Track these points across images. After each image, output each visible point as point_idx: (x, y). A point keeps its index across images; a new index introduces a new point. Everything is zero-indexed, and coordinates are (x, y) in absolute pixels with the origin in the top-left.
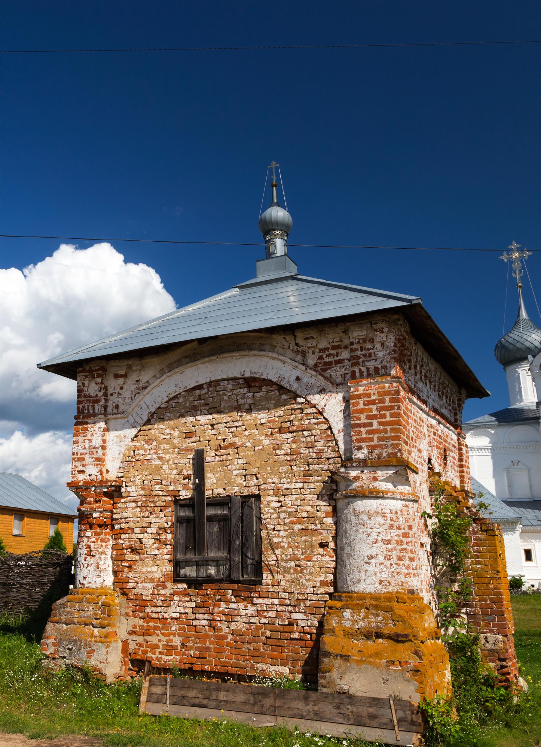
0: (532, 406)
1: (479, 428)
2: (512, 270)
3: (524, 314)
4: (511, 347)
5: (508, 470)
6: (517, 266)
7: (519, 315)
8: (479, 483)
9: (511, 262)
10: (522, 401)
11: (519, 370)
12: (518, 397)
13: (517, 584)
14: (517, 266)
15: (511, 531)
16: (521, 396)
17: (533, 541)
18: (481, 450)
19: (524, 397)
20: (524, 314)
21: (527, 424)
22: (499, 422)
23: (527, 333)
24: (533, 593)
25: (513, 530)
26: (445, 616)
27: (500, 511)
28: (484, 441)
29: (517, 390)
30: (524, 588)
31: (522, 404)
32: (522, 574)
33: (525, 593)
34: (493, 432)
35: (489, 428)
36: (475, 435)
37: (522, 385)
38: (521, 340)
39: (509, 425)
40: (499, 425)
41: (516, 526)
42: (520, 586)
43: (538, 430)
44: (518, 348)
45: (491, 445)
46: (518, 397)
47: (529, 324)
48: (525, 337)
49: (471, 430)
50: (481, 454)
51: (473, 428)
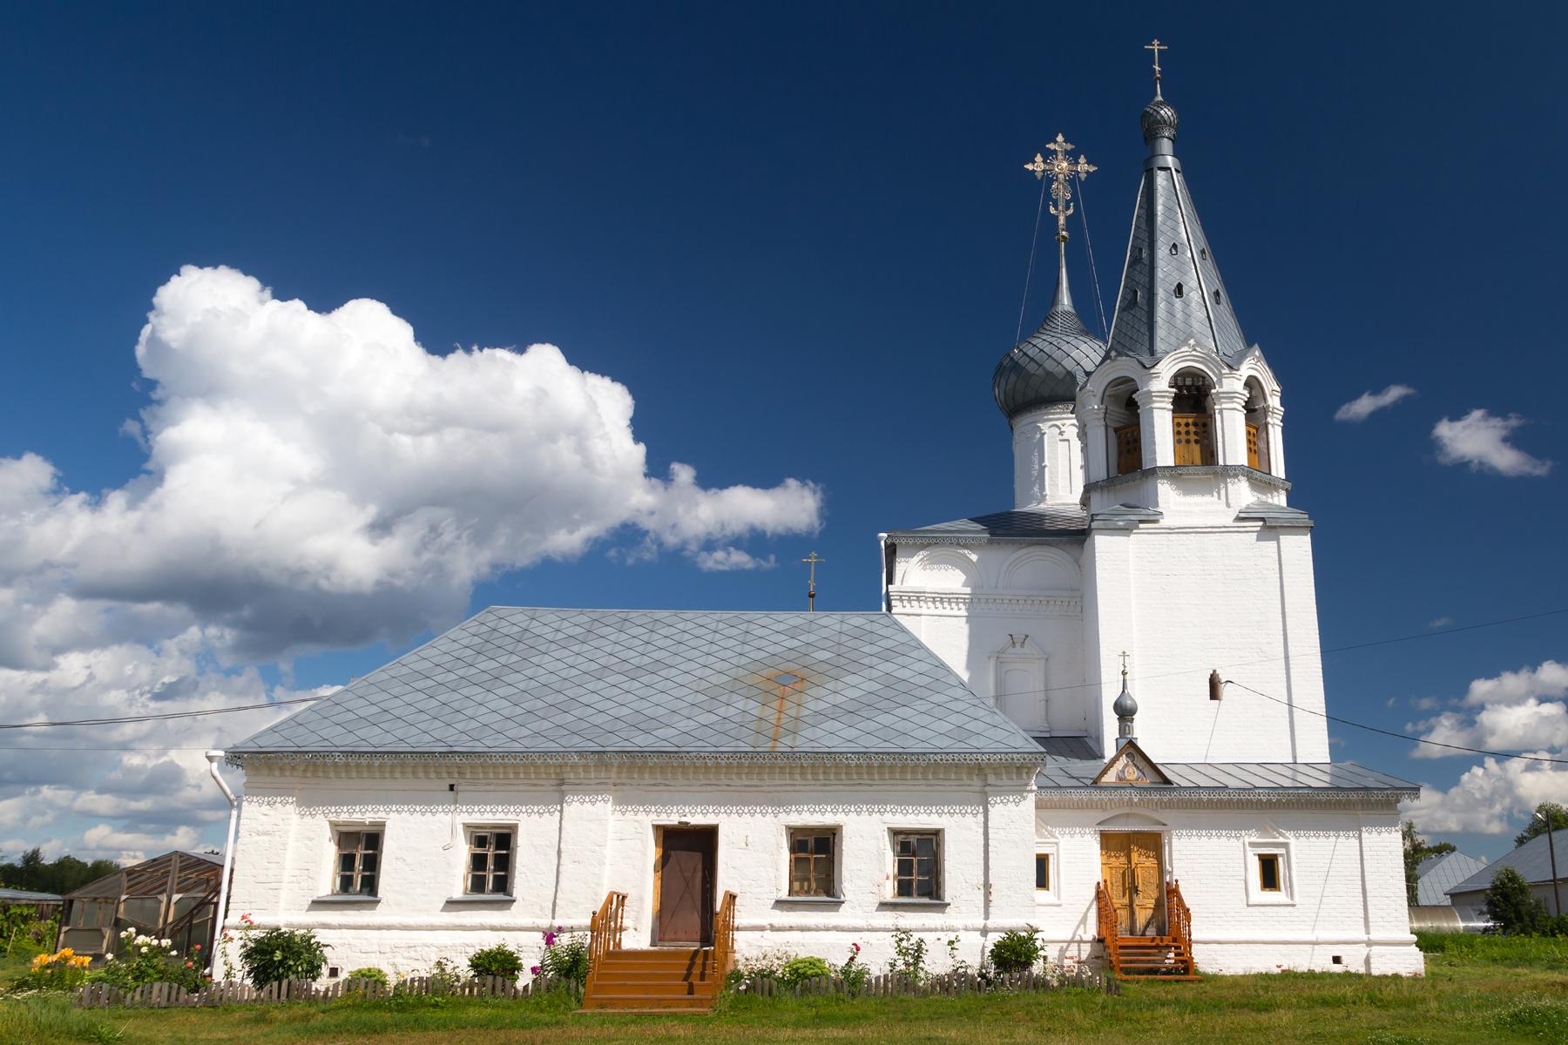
0: (1073, 508)
1: (943, 545)
2: (1050, 199)
3: (1065, 300)
4: (1032, 368)
5: (1000, 661)
6: (1061, 191)
7: (1054, 299)
8: (937, 658)
9: (1049, 179)
10: (1043, 498)
11: (1044, 427)
12: (1036, 489)
13: (1018, 955)
14: (1061, 191)
15: (1014, 792)
16: (1042, 488)
17: (1057, 831)
18: (942, 601)
19: (1047, 491)
20: (1065, 300)
21: (1056, 545)
22: (992, 534)
23: (1070, 339)
24: (1062, 984)
25: (1021, 791)
26: (1452, 1010)
27: (990, 732)
28: (951, 580)
29: (1035, 473)
30: (1037, 968)
31: (1042, 506)
32: (1035, 923)
33: (1040, 984)
34: (974, 557)
35: (965, 547)
36: (933, 562)
37: (1046, 462)
38: (1057, 354)
39: (1014, 543)
40: (990, 542)
41: (1029, 778)
42: (1028, 964)
43: (1077, 561)
44: (1049, 373)
45: (968, 590)
46: (1036, 489)
47: (1075, 323)
48: (1065, 347)
49: (923, 547)
50: (940, 611)
51: (929, 545)
